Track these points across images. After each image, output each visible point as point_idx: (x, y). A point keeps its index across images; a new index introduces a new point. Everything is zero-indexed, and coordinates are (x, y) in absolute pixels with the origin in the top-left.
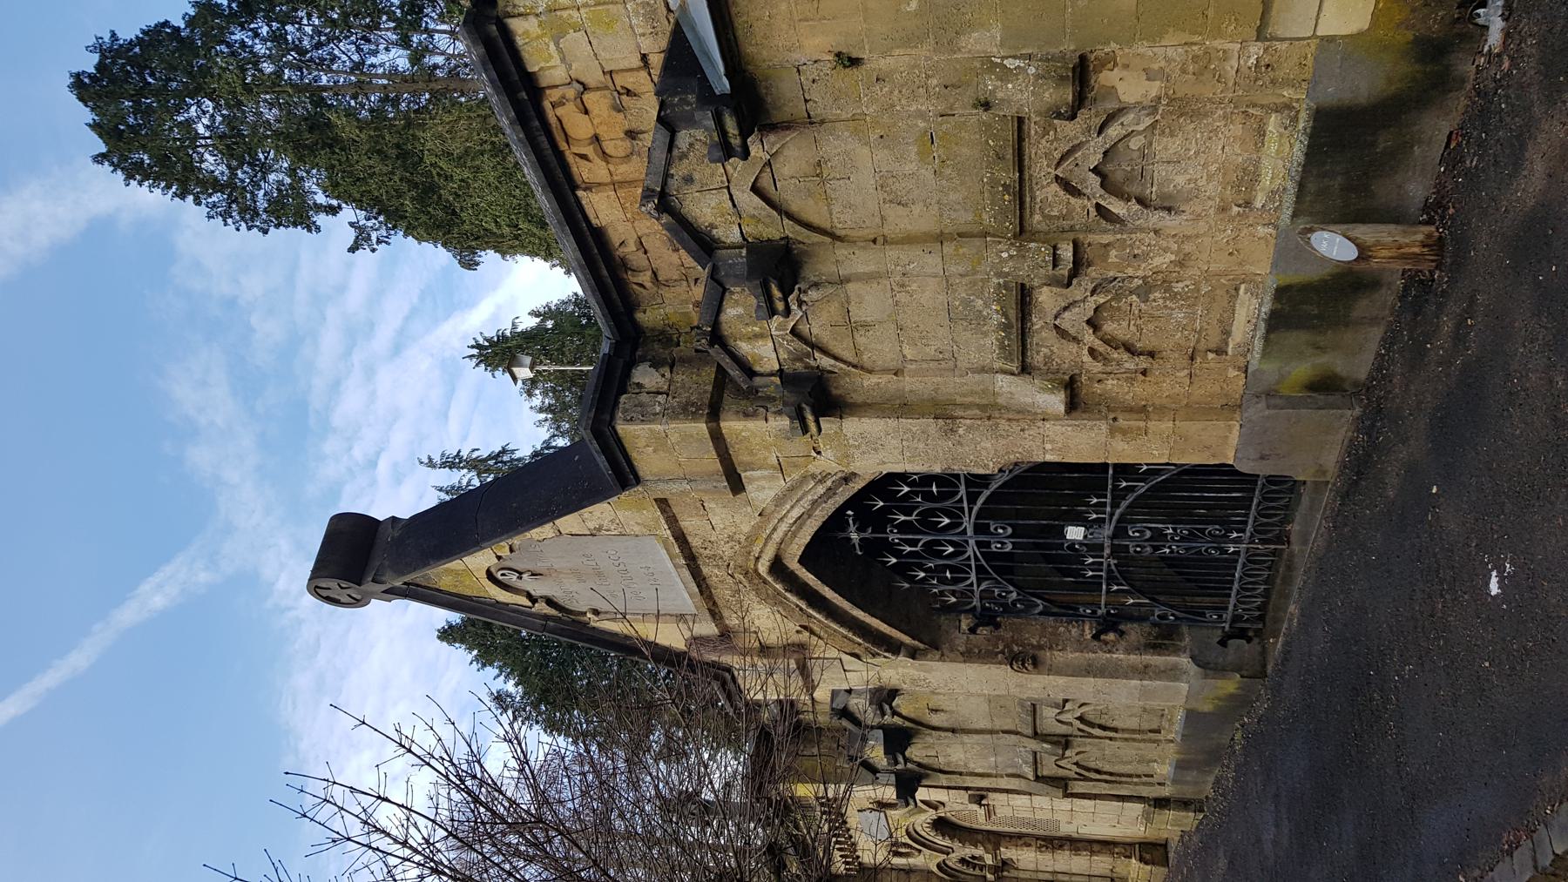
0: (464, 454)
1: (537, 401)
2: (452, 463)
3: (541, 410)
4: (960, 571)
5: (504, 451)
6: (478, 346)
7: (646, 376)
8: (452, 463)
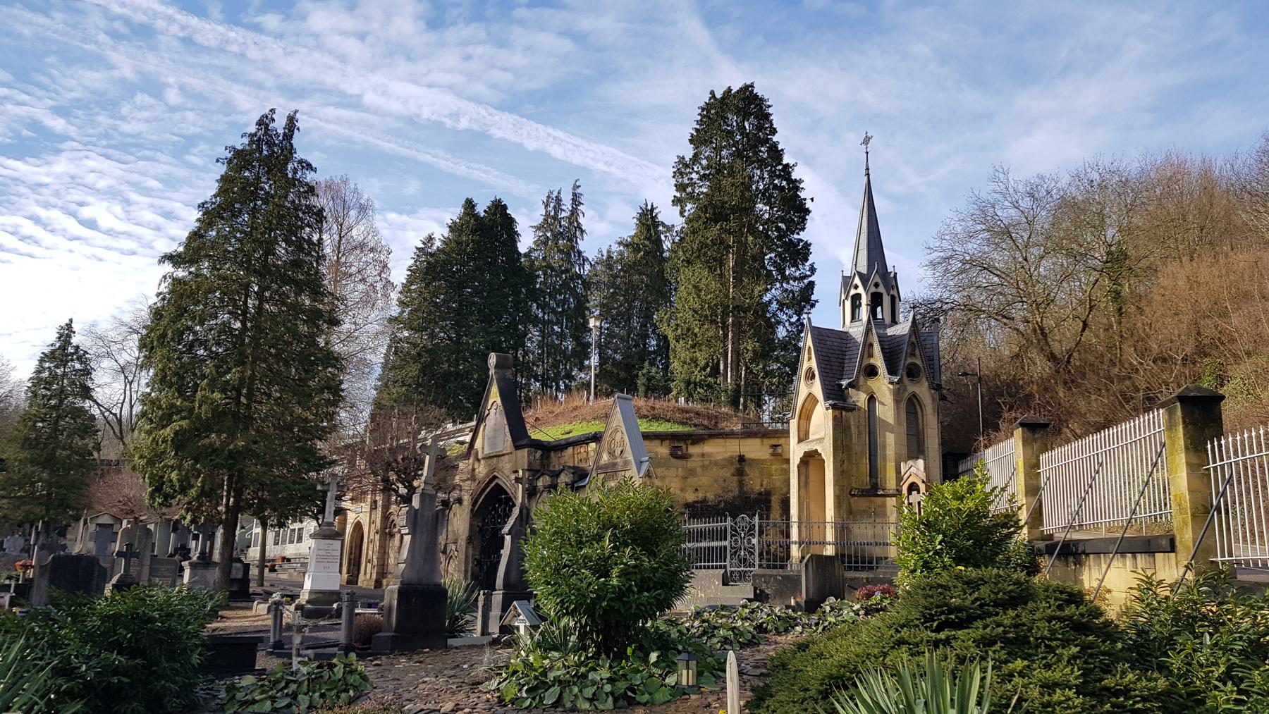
0: (581, 207)
1: (615, 248)
2: (576, 200)
3: (609, 252)
4: (493, 523)
5: (582, 231)
6: (653, 209)
7: (539, 453)
8: (576, 200)
